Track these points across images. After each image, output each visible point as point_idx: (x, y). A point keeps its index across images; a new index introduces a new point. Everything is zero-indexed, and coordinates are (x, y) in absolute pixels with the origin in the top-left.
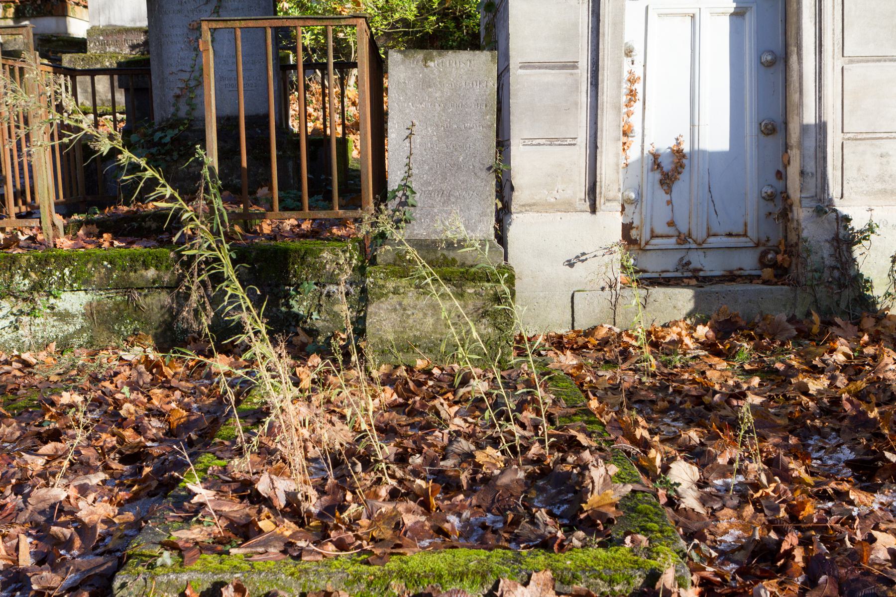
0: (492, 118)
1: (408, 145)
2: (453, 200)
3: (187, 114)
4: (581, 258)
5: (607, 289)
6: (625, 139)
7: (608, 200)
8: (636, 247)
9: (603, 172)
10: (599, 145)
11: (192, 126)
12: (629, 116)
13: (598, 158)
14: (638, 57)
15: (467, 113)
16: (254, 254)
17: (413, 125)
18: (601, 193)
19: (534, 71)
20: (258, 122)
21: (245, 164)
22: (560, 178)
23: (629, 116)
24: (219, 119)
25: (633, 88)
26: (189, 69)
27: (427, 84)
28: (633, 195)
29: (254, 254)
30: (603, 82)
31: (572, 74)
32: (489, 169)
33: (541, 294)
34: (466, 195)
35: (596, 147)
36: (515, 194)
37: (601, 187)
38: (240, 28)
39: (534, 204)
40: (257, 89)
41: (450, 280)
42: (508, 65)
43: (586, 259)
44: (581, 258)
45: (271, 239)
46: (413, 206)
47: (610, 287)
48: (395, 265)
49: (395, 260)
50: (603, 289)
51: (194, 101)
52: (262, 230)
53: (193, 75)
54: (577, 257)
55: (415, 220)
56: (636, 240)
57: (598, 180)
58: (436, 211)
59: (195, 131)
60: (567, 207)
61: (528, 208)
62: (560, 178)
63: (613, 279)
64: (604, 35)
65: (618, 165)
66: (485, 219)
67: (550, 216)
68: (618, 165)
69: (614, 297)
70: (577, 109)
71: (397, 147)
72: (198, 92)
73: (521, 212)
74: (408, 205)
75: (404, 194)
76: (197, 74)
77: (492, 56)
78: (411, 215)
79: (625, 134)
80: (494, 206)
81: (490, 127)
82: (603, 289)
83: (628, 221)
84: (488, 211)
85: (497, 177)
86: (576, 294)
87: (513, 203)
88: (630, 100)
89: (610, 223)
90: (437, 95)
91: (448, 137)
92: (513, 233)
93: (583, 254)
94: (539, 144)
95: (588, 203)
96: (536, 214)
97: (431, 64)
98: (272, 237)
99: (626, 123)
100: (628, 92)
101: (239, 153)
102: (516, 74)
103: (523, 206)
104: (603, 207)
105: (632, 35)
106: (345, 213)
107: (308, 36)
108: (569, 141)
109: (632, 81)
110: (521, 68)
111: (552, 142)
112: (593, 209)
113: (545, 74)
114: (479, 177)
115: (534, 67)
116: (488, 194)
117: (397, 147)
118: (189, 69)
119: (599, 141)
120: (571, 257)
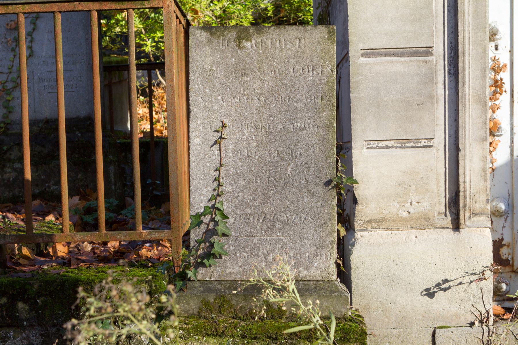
0: (329, 115)
1: (217, 152)
2: (279, 226)
3: (4, 117)
4: (443, 286)
5: (477, 323)
6: (490, 139)
7: (475, 214)
8: (508, 269)
9: (467, 179)
10: (461, 146)
11: (8, 129)
12: (494, 112)
13: (461, 162)
14: (504, 41)
15: (296, 109)
16: (36, 286)
17: (224, 126)
18: (465, 205)
19: (379, 59)
20: (80, 125)
21: (28, 175)
22: (413, 187)
23: (494, 112)
24: (67, 120)
25: (499, 78)
26: (7, 71)
27: (242, 71)
28: (502, 206)
29: (36, 286)
30: (464, 70)
31: (425, 62)
32: (328, 183)
33: (394, 332)
34: (297, 220)
35: (458, 150)
36: (359, 208)
37: (465, 198)
38: (24, 13)
39: (382, 220)
40: (80, 90)
41: (276, 339)
42: (348, 53)
43: (449, 288)
44: (443, 286)
45: (64, 264)
46: (224, 235)
47: (481, 322)
48: (200, 317)
49: (200, 311)
50: (472, 324)
51: (11, 104)
52: (55, 252)
53: (11, 76)
54: (438, 285)
55: (226, 254)
56: (507, 260)
57: (461, 189)
58: (256, 241)
59: (11, 135)
60: (424, 223)
61: (375, 225)
62: (413, 187)
63: (484, 312)
64: (463, 13)
65: (485, 171)
66: (323, 251)
67: (402, 235)
68: (485, 171)
69: (486, 334)
70: (432, 103)
71: (202, 155)
72: (16, 94)
73: (367, 229)
74: (217, 235)
75: (212, 220)
76: (15, 75)
77: (329, 32)
78: (222, 247)
79: (492, 134)
80: (335, 235)
81: (328, 127)
82: (472, 324)
83: (498, 237)
84: (328, 240)
85: (339, 194)
86: (438, 331)
87: (356, 219)
88: (495, 92)
89: (478, 241)
90: (256, 85)
91: (271, 141)
92: (358, 256)
93: (446, 281)
94: (387, 147)
95: (449, 218)
96: (385, 233)
97: (248, 44)
98: (66, 262)
99: (492, 120)
100: (492, 82)
101: (58, 158)
102: (358, 62)
103: (369, 222)
104: (468, 223)
105: (497, 16)
106: (150, 234)
107: (149, 43)
108: (423, 143)
109: (497, 70)
110: (362, 55)
111: (402, 143)
112: (456, 226)
113: (392, 62)
114: (313, 195)
115: (380, 55)
116: (326, 217)
117: (202, 155)
118: (7, 71)
119: (461, 141)
120: (431, 284)
